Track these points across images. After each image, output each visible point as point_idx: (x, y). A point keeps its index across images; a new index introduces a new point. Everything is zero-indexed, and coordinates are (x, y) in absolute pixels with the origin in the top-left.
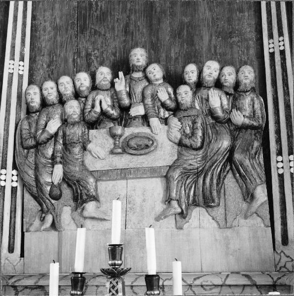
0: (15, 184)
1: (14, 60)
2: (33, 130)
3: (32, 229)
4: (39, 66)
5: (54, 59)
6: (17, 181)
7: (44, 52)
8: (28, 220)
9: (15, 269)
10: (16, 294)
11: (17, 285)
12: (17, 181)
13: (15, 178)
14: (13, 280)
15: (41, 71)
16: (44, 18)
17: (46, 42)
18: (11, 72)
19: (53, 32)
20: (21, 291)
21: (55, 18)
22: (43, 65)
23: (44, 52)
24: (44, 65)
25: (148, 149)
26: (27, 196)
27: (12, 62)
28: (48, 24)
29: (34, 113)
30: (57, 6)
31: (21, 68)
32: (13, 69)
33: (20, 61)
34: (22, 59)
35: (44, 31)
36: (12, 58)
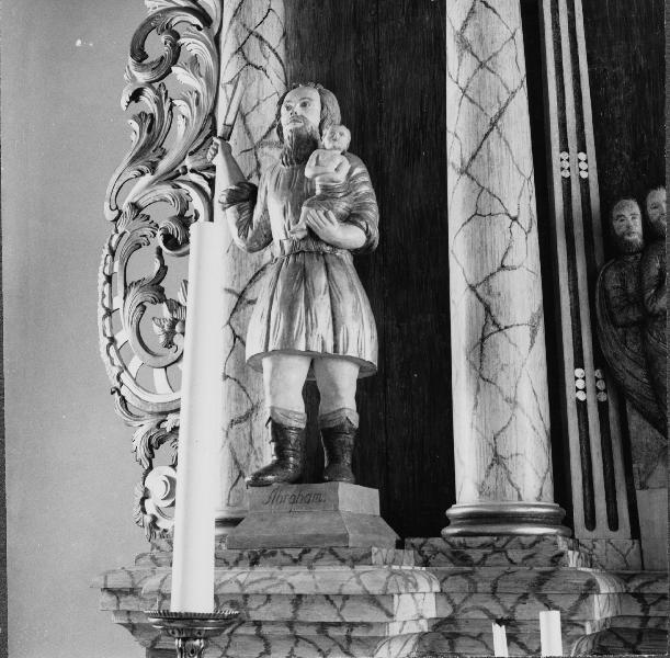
0: (603, 397)
1: (567, 150)
2: (631, 289)
3: (652, 482)
4: (614, 159)
5: (646, 141)
6: (605, 391)
7: (621, 129)
8: (642, 466)
9: (626, 561)
10: (325, 656)
11: (646, 592)
12: (605, 391)
13: (601, 385)
14: (637, 583)
15: (619, 167)
16: (610, 57)
17: (621, 108)
18: (567, 176)
19: (634, 87)
20: (654, 604)
21: (635, 57)
22: (621, 155)
23: (621, 129)
24: (624, 153)
25: (347, 288)
26: (635, 420)
27: (565, 155)
28: (620, 69)
29: (632, 254)
30: (636, 31)
31: (583, 166)
32: (569, 169)
33: (579, 152)
34: (582, 148)
35: (616, 83)
36: (565, 148)
